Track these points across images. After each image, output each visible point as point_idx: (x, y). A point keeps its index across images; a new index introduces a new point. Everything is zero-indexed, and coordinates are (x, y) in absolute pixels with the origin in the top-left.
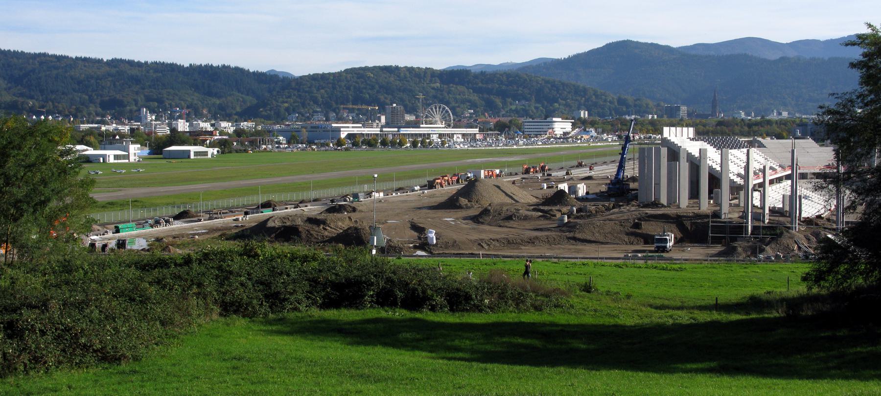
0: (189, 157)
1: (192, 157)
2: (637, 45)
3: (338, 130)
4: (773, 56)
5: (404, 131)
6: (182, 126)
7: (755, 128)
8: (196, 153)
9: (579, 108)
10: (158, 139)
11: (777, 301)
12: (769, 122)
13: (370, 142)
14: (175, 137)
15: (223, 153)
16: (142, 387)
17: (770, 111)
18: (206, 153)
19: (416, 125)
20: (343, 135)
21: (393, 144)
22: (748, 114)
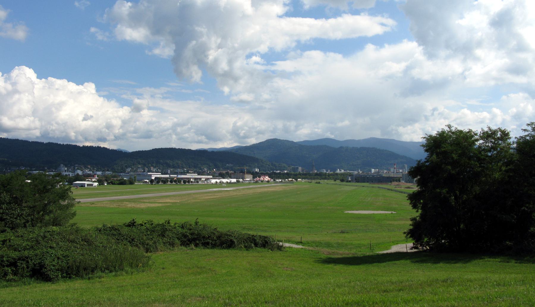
0: (85, 186)
1: (86, 186)
2: (279, 141)
3: (151, 176)
4: (337, 146)
5: (180, 176)
6: (80, 172)
7: (331, 177)
8: (88, 185)
9: (255, 168)
10: (70, 178)
11: (218, 246)
12: (337, 174)
13: (165, 181)
14: (78, 178)
15: (99, 185)
16: (377, 303)
17: (336, 170)
18: (92, 185)
19: (184, 173)
20: (153, 178)
21: (175, 181)
22: (327, 171)
